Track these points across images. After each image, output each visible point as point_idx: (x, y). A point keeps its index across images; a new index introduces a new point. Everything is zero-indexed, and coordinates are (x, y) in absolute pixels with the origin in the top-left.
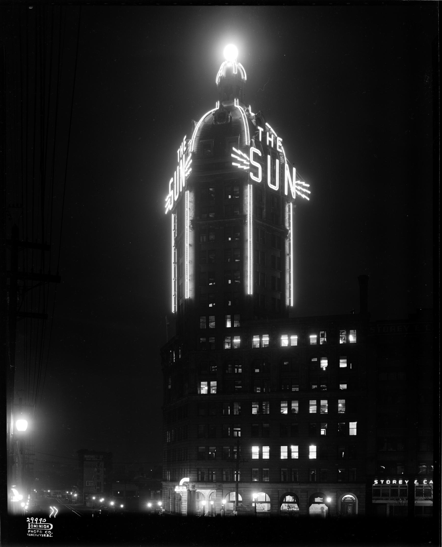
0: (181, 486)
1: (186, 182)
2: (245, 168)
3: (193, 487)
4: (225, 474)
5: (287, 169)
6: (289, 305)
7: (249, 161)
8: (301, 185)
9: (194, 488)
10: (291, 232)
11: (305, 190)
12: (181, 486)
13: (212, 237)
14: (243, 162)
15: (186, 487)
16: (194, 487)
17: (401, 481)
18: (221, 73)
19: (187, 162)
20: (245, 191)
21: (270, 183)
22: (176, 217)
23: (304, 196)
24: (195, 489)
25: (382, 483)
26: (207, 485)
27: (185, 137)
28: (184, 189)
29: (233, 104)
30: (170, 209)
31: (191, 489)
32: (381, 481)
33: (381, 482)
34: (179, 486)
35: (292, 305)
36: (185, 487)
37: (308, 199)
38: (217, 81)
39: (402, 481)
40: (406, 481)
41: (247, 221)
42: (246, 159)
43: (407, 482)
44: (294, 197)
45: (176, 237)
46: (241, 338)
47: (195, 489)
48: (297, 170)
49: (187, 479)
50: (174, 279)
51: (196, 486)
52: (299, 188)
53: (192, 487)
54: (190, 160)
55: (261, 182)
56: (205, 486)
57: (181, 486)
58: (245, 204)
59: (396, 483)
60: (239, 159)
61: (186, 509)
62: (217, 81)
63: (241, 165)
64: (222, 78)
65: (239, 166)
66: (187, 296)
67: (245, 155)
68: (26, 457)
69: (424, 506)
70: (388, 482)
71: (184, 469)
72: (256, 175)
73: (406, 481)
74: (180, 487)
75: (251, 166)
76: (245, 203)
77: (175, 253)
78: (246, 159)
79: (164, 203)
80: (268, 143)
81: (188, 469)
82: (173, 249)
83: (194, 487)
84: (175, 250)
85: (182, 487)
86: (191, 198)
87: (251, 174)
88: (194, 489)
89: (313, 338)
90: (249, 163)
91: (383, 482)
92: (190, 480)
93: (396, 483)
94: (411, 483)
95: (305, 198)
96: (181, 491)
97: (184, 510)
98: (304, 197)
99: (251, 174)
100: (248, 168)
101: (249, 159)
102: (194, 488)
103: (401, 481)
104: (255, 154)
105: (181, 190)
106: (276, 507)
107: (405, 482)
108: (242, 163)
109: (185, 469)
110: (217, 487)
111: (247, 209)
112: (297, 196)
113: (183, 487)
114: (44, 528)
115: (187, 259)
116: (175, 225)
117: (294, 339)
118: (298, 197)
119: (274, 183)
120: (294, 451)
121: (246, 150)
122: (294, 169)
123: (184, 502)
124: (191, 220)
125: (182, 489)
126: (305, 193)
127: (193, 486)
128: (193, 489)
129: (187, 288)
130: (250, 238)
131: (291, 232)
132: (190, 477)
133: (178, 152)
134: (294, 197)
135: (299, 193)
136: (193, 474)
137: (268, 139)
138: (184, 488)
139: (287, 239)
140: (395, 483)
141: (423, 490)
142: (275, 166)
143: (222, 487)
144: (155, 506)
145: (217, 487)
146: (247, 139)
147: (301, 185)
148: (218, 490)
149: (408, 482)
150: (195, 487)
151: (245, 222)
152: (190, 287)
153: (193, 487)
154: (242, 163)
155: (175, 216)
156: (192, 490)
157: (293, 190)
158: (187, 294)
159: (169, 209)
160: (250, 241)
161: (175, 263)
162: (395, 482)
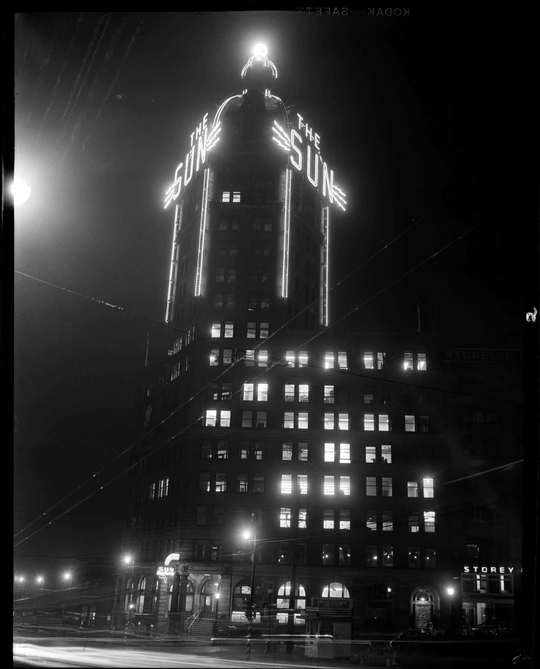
0: (167, 568)
1: (207, 157)
3: (185, 570)
5: (325, 169)
6: (322, 324)
7: (290, 143)
8: (338, 191)
9: (187, 572)
10: (327, 238)
11: (341, 198)
12: (167, 568)
13: (235, 227)
14: (284, 141)
15: (173, 569)
16: (186, 569)
17: (503, 569)
18: (249, 64)
19: (211, 135)
20: (283, 176)
21: (310, 176)
22: (181, 209)
23: (340, 205)
24: (188, 573)
25: (476, 571)
26: (207, 567)
27: (207, 114)
28: (203, 167)
29: (264, 94)
30: (174, 199)
31: (181, 573)
32: (474, 567)
33: (474, 569)
34: (163, 565)
36: (172, 568)
38: (243, 73)
39: (504, 568)
40: (509, 568)
41: (283, 210)
42: (286, 139)
43: (511, 570)
45: (179, 231)
46: (269, 354)
47: (188, 573)
49: (175, 556)
50: (171, 281)
51: (189, 568)
52: (336, 193)
53: (184, 569)
54: (218, 129)
55: (301, 170)
56: (205, 568)
57: (167, 566)
58: (282, 191)
59: (495, 572)
60: (280, 136)
61: (164, 606)
62: (243, 73)
64: (249, 70)
66: (197, 293)
67: (286, 135)
70: (485, 570)
71: (167, 541)
72: (297, 160)
73: (509, 568)
74: (165, 568)
75: (291, 148)
76: (282, 190)
77: (176, 250)
78: (286, 139)
79: (164, 196)
80: (307, 135)
81: (179, 541)
82: (174, 244)
83: (186, 569)
84: (176, 246)
85: (168, 568)
86: (211, 178)
87: (292, 158)
88: (186, 573)
89: (368, 360)
90: (289, 145)
91: (477, 569)
92: (180, 557)
93: (495, 572)
95: (341, 207)
96: (165, 575)
97: (162, 608)
98: (340, 206)
99: (292, 158)
100: (289, 150)
101: (290, 141)
102: (187, 572)
103: (503, 569)
105: (197, 169)
106: (286, 616)
107: (509, 571)
108: (283, 142)
109: (169, 541)
110: (224, 570)
111: (283, 197)
113: (169, 568)
115: (201, 247)
116: (179, 218)
118: (335, 203)
119: (313, 176)
123: (163, 595)
124: (209, 202)
125: (168, 572)
127: (185, 568)
128: (184, 573)
129: (198, 283)
130: (287, 229)
131: (327, 238)
132: (181, 553)
133: (192, 136)
135: (336, 200)
136: (185, 548)
138: (171, 571)
139: (322, 246)
140: (494, 571)
142: (314, 160)
143: (232, 571)
145: (224, 570)
147: (338, 191)
148: (224, 576)
149: (513, 571)
150: (187, 569)
151: (281, 211)
152: (203, 283)
153: (185, 569)
154: (283, 142)
155: (180, 208)
156: (183, 575)
157: (330, 194)
158: (198, 290)
159: (173, 199)
160: (287, 234)
161: (175, 260)
162: (494, 569)
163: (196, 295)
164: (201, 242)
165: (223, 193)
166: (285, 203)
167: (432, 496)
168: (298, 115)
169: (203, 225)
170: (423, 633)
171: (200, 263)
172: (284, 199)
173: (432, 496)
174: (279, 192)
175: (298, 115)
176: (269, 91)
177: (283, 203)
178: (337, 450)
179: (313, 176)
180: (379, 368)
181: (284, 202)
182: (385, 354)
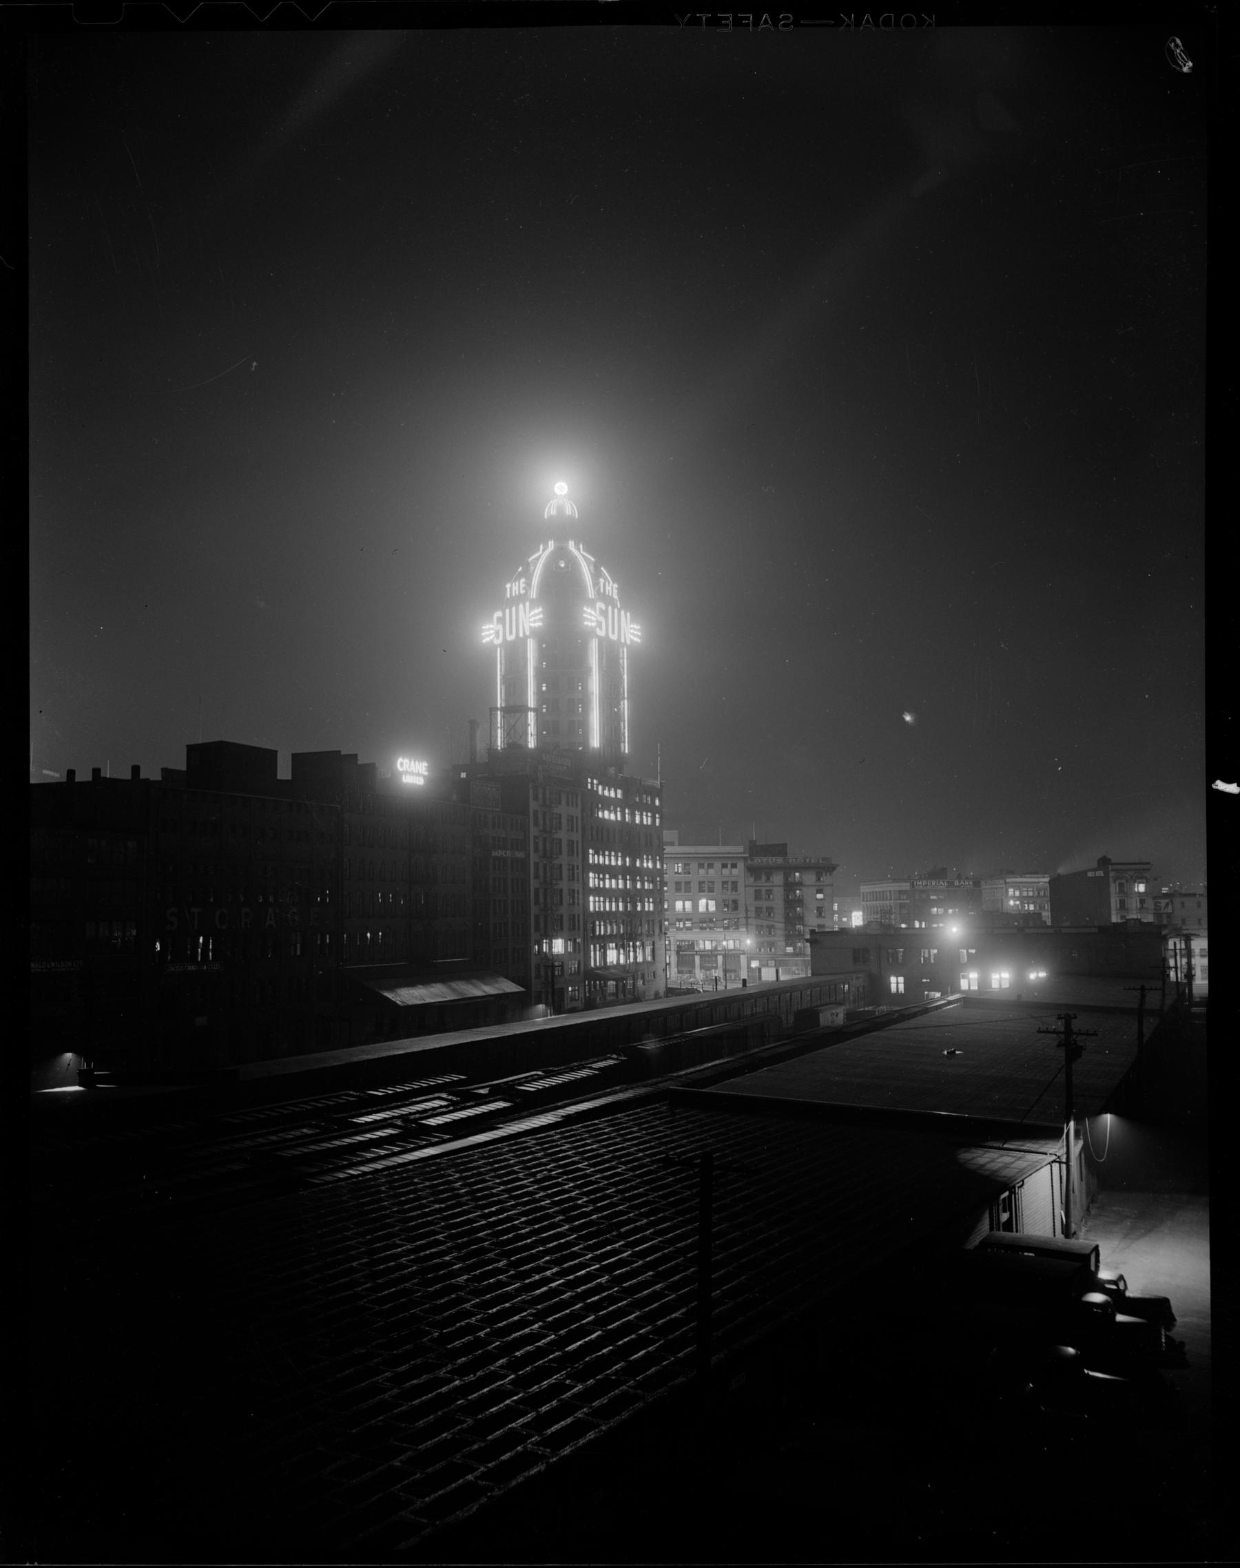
2: (594, 624)
4: (1168, 949)
35: (627, 751)
37: (639, 641)
44: (628, 642)
48: (631, 615)
63: (591, 622)
65: (590, 624)
68: (1073, 1016)
69: (718, 845)
90: (595, 619)
94: (633, 862)
104: (600, 609)
112: (632, 640)
114: (1027, 891)
117: (688, 904)
119: (613, 632)
120: (1050, 1181)
121: (593, 607)
122: (628, 614)
126: (638, 636)
134: (628, 642)
137: (607, 588)
141: (686, 1176)
144: (984, 983)
146: (591, 593)
179: (613, 632)
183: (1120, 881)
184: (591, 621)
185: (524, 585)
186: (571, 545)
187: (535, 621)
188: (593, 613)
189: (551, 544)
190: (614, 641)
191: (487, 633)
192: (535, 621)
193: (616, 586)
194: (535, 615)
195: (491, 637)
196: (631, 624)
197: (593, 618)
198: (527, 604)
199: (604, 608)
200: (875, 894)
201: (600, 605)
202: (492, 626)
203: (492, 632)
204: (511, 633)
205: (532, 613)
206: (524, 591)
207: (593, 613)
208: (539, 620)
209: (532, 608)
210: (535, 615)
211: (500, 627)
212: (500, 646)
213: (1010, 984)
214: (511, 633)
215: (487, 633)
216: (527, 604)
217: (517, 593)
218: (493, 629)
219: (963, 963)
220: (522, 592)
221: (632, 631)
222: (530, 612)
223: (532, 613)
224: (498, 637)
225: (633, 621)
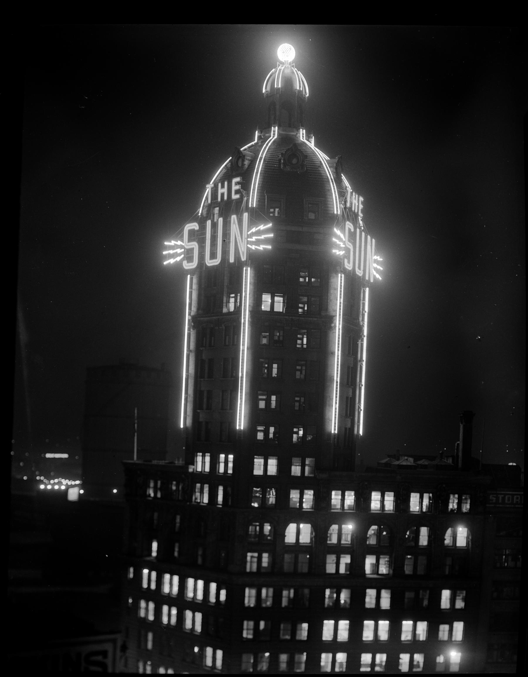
66: (240, 425)
104: (350, 230)
119: (359, 268)
134: (372, 281)
163: (238, 428)
164: (243, 362)
165: (262, 294)
166: (336, 316)
167: (262, 439)
168: (342, 174)
169: (244, 342)
170: (134, 573)
171: (242, 389)
172: (336, 311)
173: (262, 439)
174: (329, 301)
175: (342, 174)
176: (304, 131)
177: (334, 316)
178: (378, 598)
179: (359, 268)
180: (424, 509)
181: (335, 314)
182: (431, 495)
183: (519, 498)
184: (340, 249)
185: (238, 187)
186: (302, 135)
187: (258, 242)
188: (342, 236)
189: (275, 132)
190: (359, 277)
191: (171, 252)
192: (258, 242)
193: (361, 199)
194: (259, 233)
195: (178, 259)
196: (375, 255)
197: (342, 245)
198: (246, 215)
199: (352, 230)
200: (346, 535)
201: (349, 225)
202: (179, 243)
203: (179, 251)
204: (213, 256)
205: (254, 230)
206: (238, 196)
207: (342, 236)
208: (266, 241)
209: (253, 222)
210: (259, 233)
211: (195, 245)
212: (192, 272)
213: (459, 652)
214: (213, 256)
215: (171, 252)
216: (246, 215)
217: (226, 198)
218: (181, 247)
219: (442, 639)
220: (235, 197)
221: (254, 239)
222: (249, 228)
223: (254, 230)
224: (189, 258)
225: (379, 249)
